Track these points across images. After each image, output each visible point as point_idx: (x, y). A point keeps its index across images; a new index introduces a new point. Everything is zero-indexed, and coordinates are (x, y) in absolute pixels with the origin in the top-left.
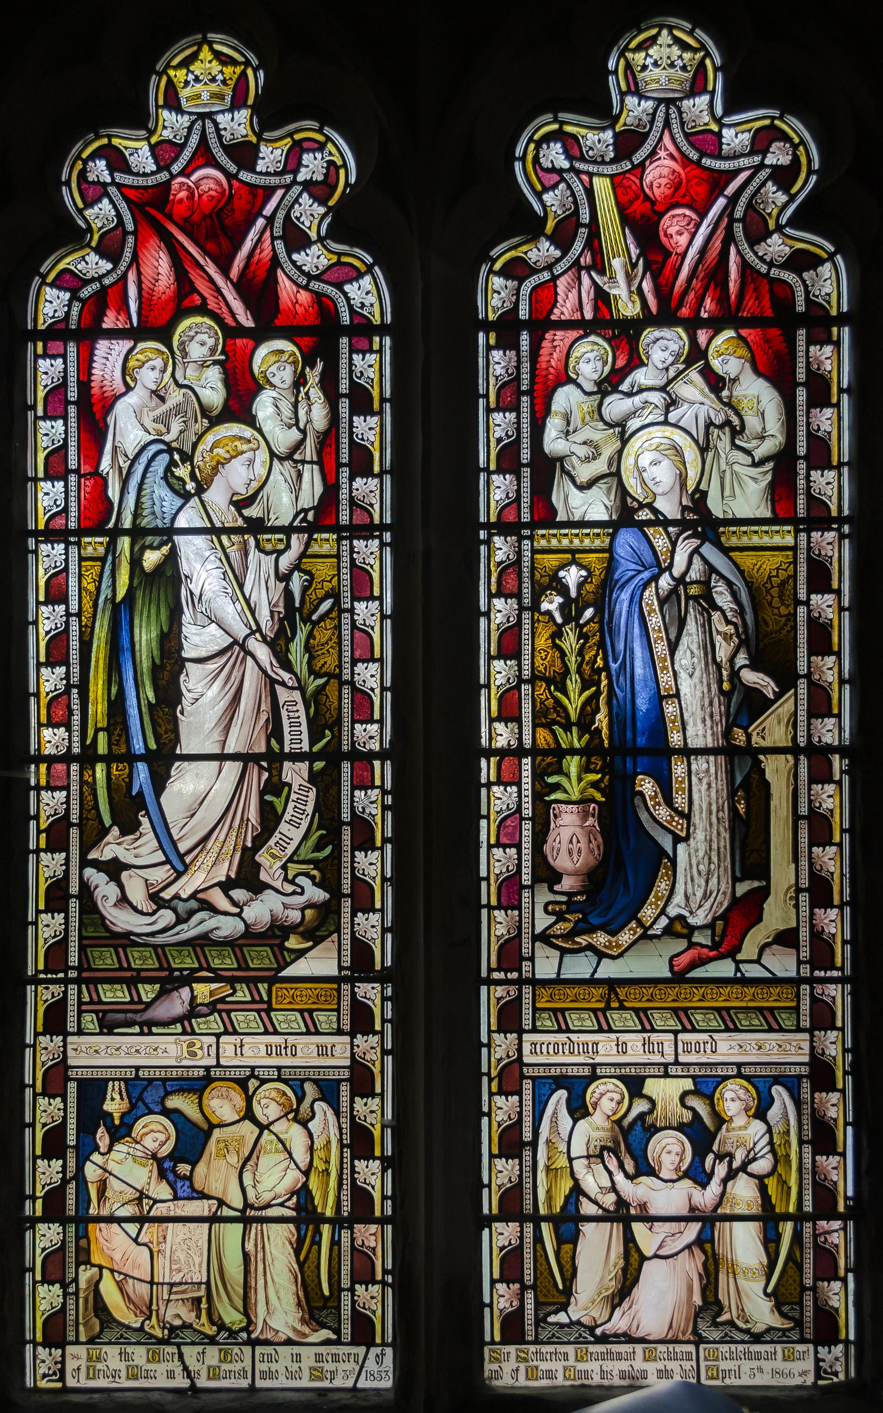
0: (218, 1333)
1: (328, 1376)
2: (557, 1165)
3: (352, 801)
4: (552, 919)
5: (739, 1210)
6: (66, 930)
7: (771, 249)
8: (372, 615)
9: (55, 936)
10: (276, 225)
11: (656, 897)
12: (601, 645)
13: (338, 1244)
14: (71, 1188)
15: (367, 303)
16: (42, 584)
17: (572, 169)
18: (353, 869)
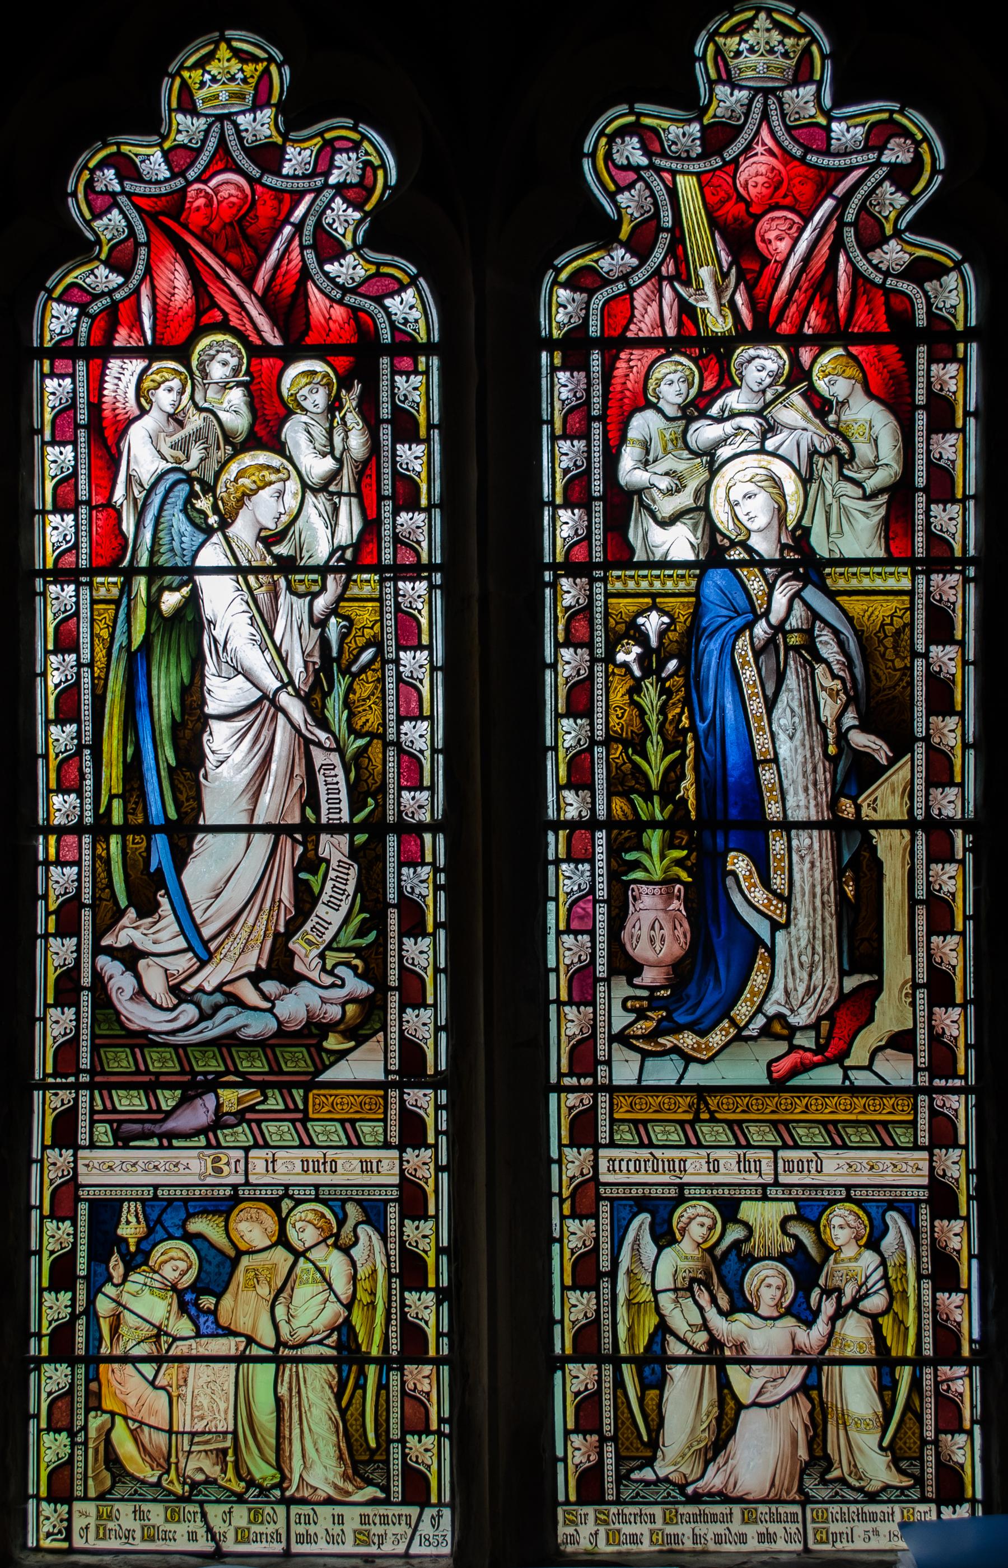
0: (247, 1490)
1: (376, 1540)
2: (639, 1299)
3: (399, 880)
4: (633, 1017)
5: (848, 1353)
6: (77, 1027)
7: (888, 257)
8: (421, 666)
9: (66, 1034)
10: (306, 232)
11: (751, 992)
12: (687, 701)
13: (387, 1387)
14: (81, 1325)
15: (411, 318)
16: (51, 630)
17: (651, 166)
18: (401, 957)
